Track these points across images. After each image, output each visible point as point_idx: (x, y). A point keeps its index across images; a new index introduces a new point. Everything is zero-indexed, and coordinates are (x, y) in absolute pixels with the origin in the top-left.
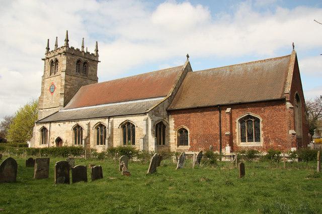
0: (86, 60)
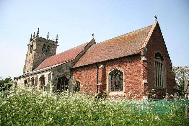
0: (49, 44)
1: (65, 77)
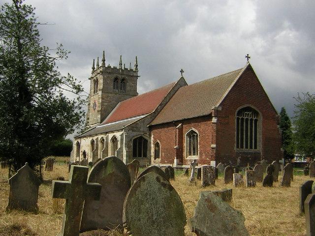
1: (143, 137)
